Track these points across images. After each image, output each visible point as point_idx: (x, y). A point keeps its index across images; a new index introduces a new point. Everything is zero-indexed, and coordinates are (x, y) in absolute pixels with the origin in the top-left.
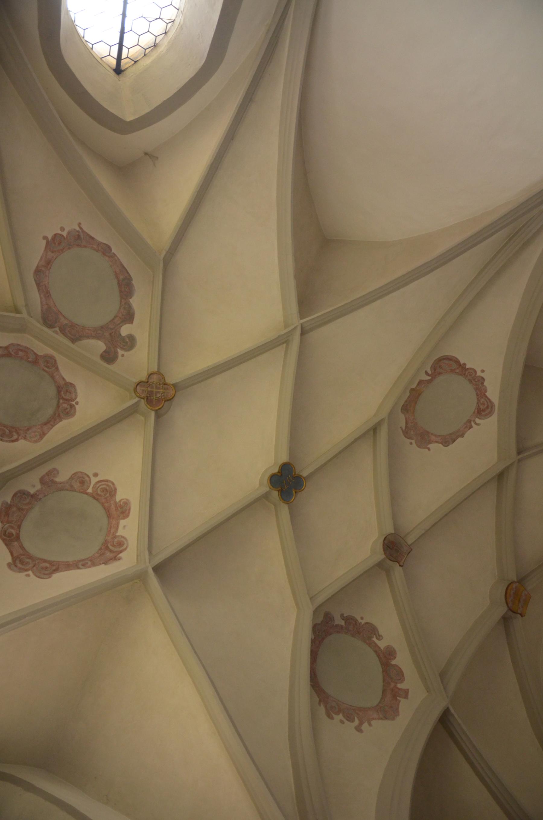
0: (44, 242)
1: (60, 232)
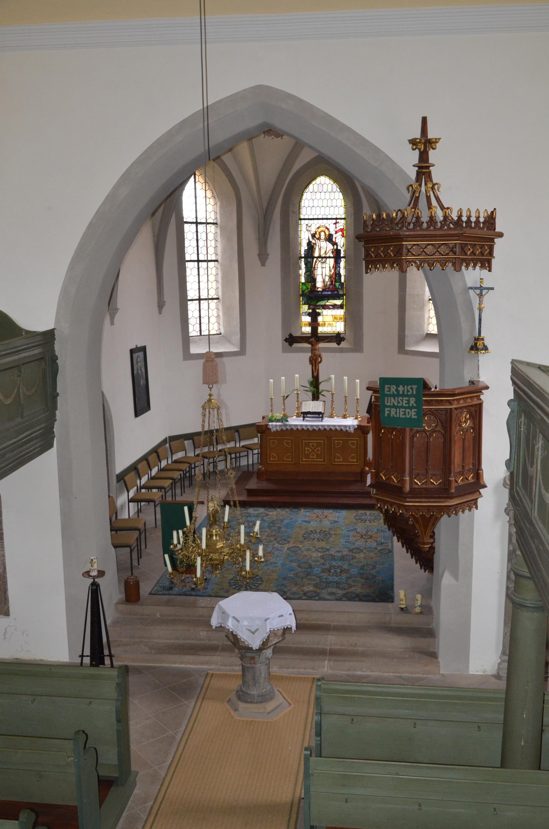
0: (283, 137)
1: (274, 138)
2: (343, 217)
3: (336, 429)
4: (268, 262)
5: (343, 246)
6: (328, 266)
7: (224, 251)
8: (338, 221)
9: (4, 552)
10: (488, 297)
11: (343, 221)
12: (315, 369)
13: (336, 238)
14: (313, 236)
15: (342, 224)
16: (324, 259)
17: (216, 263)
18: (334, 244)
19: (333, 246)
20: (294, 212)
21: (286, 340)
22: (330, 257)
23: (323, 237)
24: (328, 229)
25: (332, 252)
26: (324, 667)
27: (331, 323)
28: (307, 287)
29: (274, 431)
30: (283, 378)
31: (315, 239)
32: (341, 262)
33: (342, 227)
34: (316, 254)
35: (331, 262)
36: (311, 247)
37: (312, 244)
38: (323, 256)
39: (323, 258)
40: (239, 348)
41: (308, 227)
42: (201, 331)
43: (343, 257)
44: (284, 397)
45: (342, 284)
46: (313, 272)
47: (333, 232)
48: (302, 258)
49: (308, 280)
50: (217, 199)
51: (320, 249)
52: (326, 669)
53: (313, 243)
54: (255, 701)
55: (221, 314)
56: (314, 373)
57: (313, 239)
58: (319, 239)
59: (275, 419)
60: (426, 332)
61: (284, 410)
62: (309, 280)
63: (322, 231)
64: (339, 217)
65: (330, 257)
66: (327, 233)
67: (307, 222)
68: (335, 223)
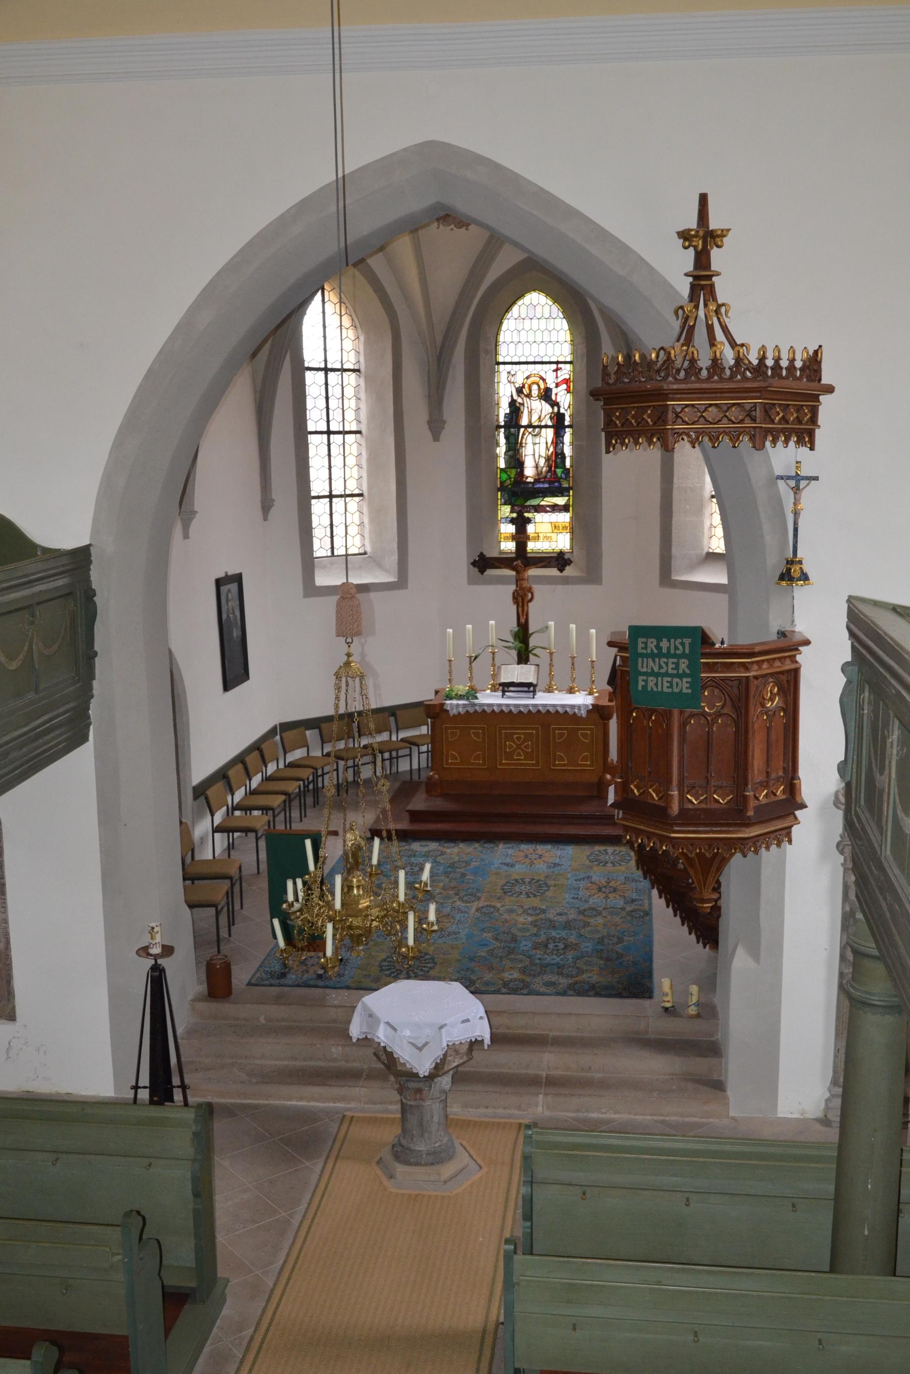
0: (469, 227)
1: (455, 229)
2: (569, 359)
3: (557, 712)
4: (444, 434)
5: (569, 407)
6: (543, 441)
7: (372, 416)
8: (560, 366)
9: (7, 916)
10: (809, 493)
11: (568, 367)
12: (523, 611)
13: (556, 394)
14: (520, 391)
15: (566, 371)
16: (537, 430)
17: (358, 435)
18: (554, 404)
19: (553, 408)
20: (487, 352)
21: (474, 564)
22: (546, 426)
23: (535, 392)
24: (544, 380)
25: (551, 418)
26: (537, 1105)
27: (548, 535)
28: (508, 475)
29: (454, 715)
30: (469, 627)
31: (522, 396)
32: (566, 435)
33: (567, 377)
34: (524, 421)
35: (549, 434)
36: (515, 409)
37: (518, 405)
38: (536, 424)
39: (535, 427)
40: (397, 576)
41: (510, 377)
42: (332, 548)
43: (568, 426)
44: (470, 657)
45: (567, 471)
46: (518, 450)
47: (551, 385)
48: (501, 427)
49: (510, 463)
50: (359, 330)
51: (530, 413)
52: (540, 1109)
53: (520, 403)
54: (423, 1162)
55: (366, 521)
56: (521, 618)
57: (519, 396)
58: (529, 396)
59: (456, 695)
60: (706, 550)
61: (471, 679)
62: (513, 464)
63: (534, 383)
64: (561, 359)
65: (546, 426)
66: (542, 386)
67: (508, 367)
68: (556, 370)
